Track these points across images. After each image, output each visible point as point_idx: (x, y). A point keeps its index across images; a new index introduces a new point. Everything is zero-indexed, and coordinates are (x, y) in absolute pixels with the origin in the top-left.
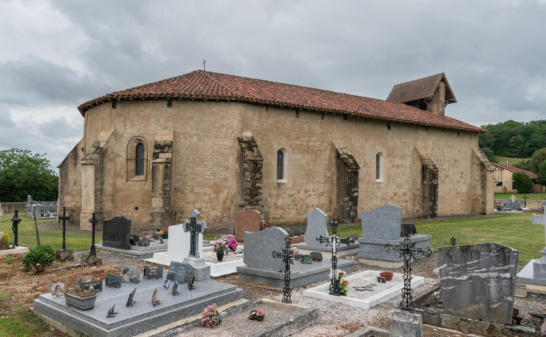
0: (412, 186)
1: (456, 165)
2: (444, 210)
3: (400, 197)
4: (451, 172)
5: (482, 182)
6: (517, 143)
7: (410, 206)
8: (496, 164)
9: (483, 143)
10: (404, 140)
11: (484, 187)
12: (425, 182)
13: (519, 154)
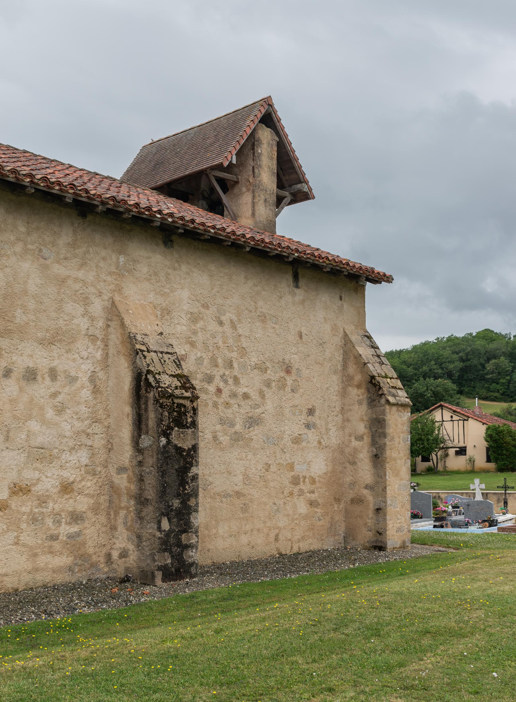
0: (102, 456)
1: (289, 382)
2: (244, 539)
3: (42, 501)
4: (269, 406)
5: (373, 443)
6: (499, 373)
7: (92, 534)
8: (454, 408)
9: (440, 371)
10: (58, 270)
11: (378, 458)
12: (146, 441)
13: (503, 394)
